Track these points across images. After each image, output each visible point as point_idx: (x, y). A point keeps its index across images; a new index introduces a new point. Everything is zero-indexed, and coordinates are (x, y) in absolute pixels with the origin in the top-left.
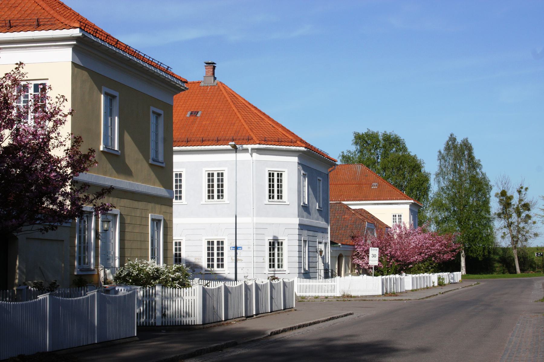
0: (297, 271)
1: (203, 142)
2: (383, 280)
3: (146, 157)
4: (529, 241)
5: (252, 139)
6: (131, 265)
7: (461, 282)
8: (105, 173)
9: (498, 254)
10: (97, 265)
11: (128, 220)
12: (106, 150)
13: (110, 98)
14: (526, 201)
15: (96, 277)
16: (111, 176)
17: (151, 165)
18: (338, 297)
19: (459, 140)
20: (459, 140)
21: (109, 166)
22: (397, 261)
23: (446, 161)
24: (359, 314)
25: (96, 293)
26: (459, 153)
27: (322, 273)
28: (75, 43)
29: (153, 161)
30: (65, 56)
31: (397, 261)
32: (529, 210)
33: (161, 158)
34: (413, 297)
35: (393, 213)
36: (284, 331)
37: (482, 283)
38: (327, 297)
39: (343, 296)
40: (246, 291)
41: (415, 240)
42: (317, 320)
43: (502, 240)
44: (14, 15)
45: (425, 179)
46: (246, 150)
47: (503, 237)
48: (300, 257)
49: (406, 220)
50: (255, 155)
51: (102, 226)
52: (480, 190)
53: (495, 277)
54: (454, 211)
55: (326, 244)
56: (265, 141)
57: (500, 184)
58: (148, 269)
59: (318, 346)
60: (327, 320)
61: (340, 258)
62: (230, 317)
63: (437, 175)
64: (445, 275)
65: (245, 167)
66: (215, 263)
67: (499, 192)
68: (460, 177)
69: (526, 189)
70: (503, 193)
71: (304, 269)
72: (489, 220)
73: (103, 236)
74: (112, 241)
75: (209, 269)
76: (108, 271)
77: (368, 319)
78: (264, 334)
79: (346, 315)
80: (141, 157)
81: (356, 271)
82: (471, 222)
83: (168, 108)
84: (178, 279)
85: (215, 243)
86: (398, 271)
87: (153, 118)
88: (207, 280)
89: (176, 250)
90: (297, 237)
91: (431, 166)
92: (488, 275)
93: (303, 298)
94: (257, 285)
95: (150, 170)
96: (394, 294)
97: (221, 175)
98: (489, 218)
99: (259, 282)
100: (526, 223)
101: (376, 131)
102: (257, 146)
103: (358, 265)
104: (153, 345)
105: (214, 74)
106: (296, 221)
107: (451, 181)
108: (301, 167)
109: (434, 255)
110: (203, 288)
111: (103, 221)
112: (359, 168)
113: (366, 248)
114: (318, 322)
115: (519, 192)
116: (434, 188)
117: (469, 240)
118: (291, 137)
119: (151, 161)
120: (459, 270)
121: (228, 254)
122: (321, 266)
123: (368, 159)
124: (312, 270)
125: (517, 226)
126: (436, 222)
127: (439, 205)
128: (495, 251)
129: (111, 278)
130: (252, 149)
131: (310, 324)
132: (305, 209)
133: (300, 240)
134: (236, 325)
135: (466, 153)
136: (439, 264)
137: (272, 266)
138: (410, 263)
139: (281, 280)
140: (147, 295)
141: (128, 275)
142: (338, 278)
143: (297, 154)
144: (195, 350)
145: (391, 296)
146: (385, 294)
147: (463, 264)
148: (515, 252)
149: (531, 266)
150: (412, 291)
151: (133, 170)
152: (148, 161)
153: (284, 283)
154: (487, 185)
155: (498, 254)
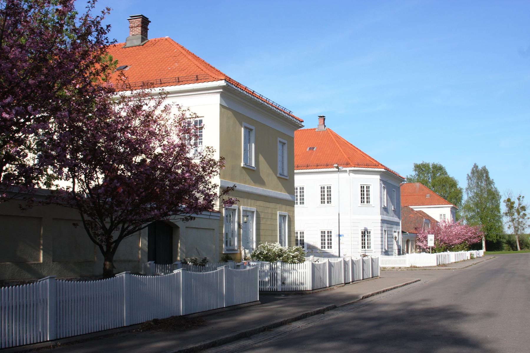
0: (380, 250)
1: (317, 166)
2: (437, 256)
3: (275, 172)
4: (525, 230)
5: (349, 164)
6: (263, 246)
7: (483, 256)
8: (245, 182)
9: (505, 239)
10: (239, 246)
11: (262, 216)
12: (245, 166)
13: (248, 131)
14: (523, 205)
15: (239, 255)
16: (249, 184)
17: (278, 178)
18: (408, 268)
19: (480, 168)
20: (480, 168)
21: (248, 178)
22: (445, 243)
23: (472, 180)
24: (425, 280)
25: (224, 268)
26: (480, 175)
27: (397, 251)
28: (222, 90)
29: (280, 175)
30: (215, 99)
31: (445, 243)
32: (525, 210)
33: (286, 173)
34: (457, 267)
35: (440, 213)
36: (373, 295)
37: (497, 257)
38: (400, 268)
39: (411, 267)
40: (345, 265)
41: (456, 230)
42: (396, 286)
43: (508, 229)
44: (182, 75)
45: (460, 191)
46: (346, 171)
47: (509, 228)
48: (382, 241)
49: (449, 217)
50: (351, 174)
51: (243, 219)
52: (493, 198)
53: (504, 253)
54: (478, 212)
55: (399, 232)
56: (358, 165)
57: (506, 194)
58: (274, 250)
59: (400, 310)
60: (403, 286)
61: (408, 242)
62: (333, 284)
63: (467, 189)
64: (474, 252)
65: (345, 183)
66: (326, 245)
67: (506, 199)
68: (482, 190)
69: (523, 197)
70: (509, 200)
71: (385, 249)
72: (500, 217)
73: (244, 226)
74: (251, 230)
75: (323, 249)
76: (247, 251)
77: (432, 285)
78: (357, 298)
79: (416, 282)
80: (271, 172)
81: (418, 250)
82: (488, 219)
83: (291, 139)
84: (297, 256)
85: (326, 233)
86: (445, 250)
87: (279, 146)
88: (318, 256)
89: (301, 237)
90: (380, 228)
91: (463, 184)
92: (492, 252)
93: (384, 268)
94: (352, 261)
95: (278, 181)
96: (444, 265)
97: (329, 188)
98: (499, 216)
99: (354, 259)
100: (523, 218)
101: (428, 162)
102: (353, 168)
103: (419, 246)
104: (272, 308)
105: (324, 123)
106: (379, 217)
107: (476, 193)
108: (382, 182)
109: (467, 240)
110: (312, 263)
111: (243, 216)
112: (418, 184)
113: (425, 235)
114: (397, 287)
115: (519, 199)
116: (465, 197)
117: (487, 230)
118: (375, 163)
119: (278, 175)
120: (481, 249)
121: (335, 239)
122: (395, 247)
123: (423, 180)
124: (390, 250)
125: (518, 221)
126: (467, 219)
127: (468, 208)
128: (503, 237)
129: (249, 256)
130: (350, 171)
131: (391, 289)
132: (385, 209)
133: (382, 230)
134: (337, 290)
135: (484, 175)
136: (470, 245)
137: (363, 247)
138: (453, 245)
139: (369, 257)
140: (271, 268)
141: (260, 253)
142: (407, 254)
143: (380, 173)
144: (301, 314)
145: (442, 266)
146: (439, 265)
147: (484, 245)
148: (517, 237)
149: (526, 246)
150: (455, 263)
151: (265, 180)
152: (276, 174)
153: (372, 259)
154: (498, 195)
155: (505, 239)
